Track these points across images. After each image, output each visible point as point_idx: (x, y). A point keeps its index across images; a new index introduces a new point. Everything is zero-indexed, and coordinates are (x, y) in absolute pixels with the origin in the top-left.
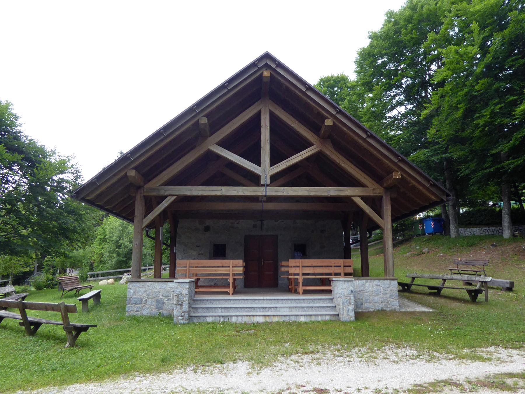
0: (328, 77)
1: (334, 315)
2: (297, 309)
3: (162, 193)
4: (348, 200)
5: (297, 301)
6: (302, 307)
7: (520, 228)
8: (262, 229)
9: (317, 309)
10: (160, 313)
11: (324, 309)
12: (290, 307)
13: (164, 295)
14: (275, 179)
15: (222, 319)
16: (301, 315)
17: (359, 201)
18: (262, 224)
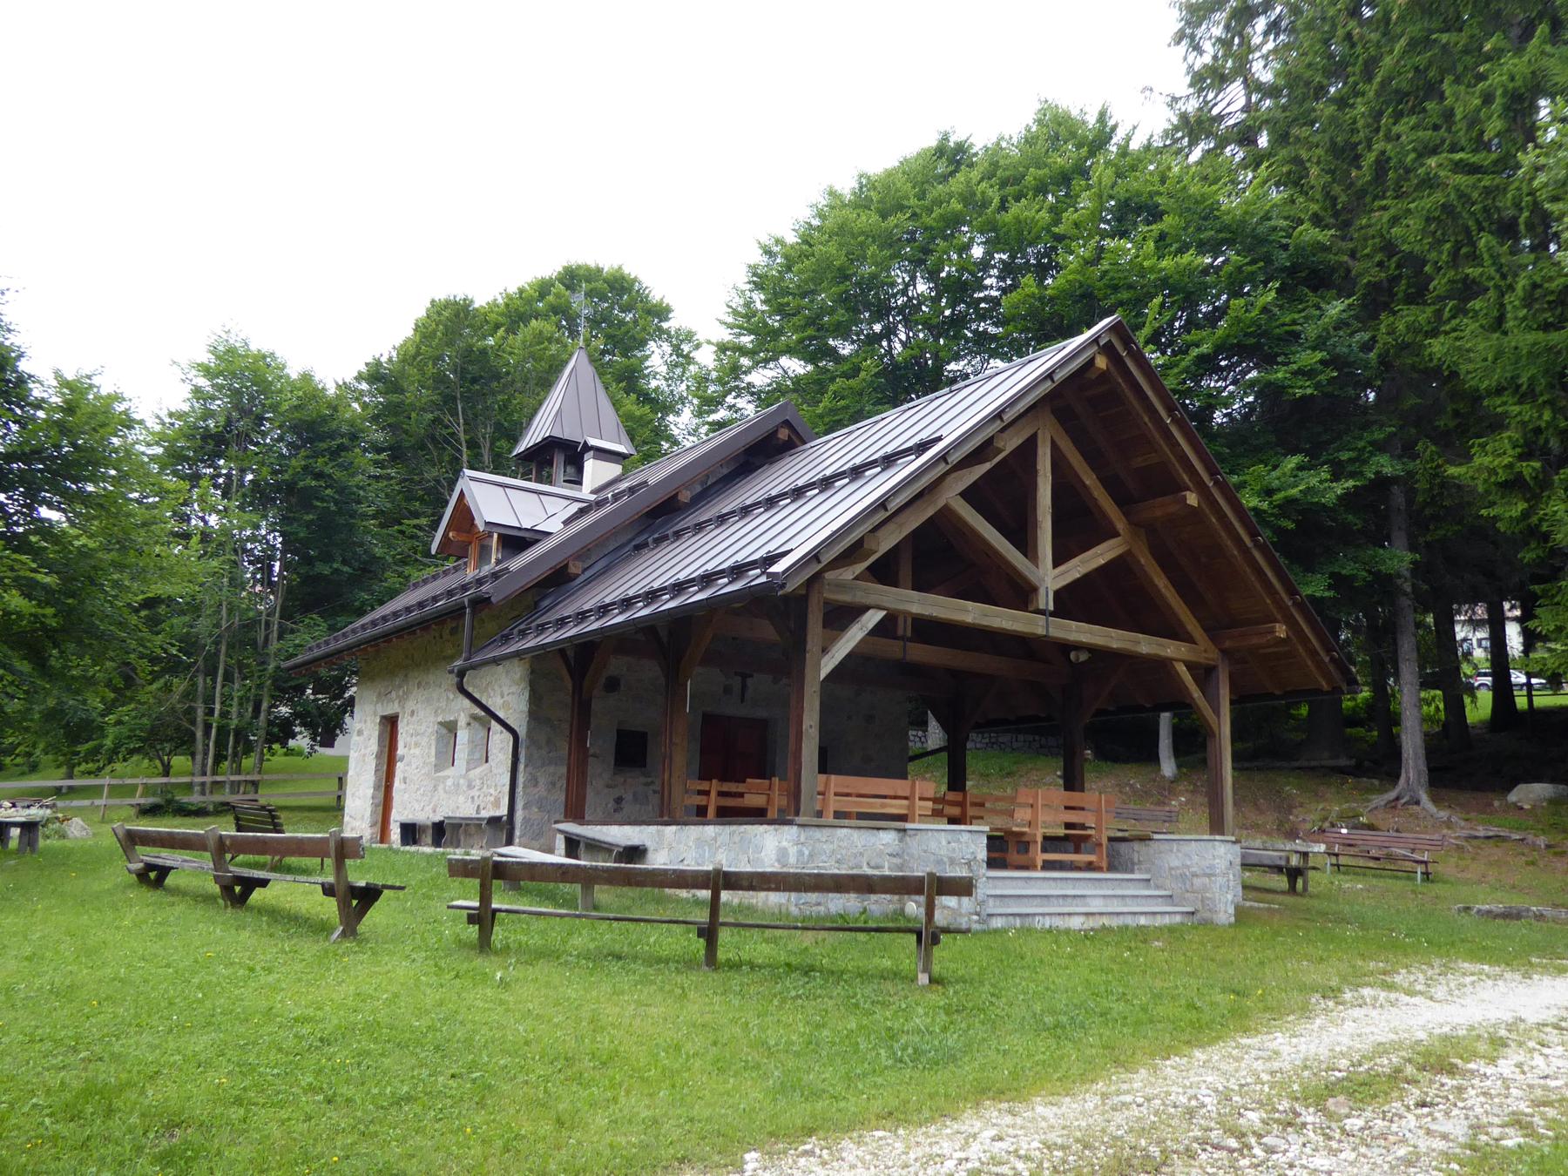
0: (588, 269)
1: (1187, 913)
2: (1115, 901)
3: (859, 598)
4: (1161, 666)
5: (1097, 883)
6: (1123, 897)
7: (1001, 740)
8: (742, 701)
9: (1144, 901)
10: (865, 910)
11: (1155, 901)
12: (1104, 896)
13: (872, 864)
14: (1071, 602)
15: (1018, 922)
16: (1142, 913)
17: (1182, 669)
18: (744, 687)
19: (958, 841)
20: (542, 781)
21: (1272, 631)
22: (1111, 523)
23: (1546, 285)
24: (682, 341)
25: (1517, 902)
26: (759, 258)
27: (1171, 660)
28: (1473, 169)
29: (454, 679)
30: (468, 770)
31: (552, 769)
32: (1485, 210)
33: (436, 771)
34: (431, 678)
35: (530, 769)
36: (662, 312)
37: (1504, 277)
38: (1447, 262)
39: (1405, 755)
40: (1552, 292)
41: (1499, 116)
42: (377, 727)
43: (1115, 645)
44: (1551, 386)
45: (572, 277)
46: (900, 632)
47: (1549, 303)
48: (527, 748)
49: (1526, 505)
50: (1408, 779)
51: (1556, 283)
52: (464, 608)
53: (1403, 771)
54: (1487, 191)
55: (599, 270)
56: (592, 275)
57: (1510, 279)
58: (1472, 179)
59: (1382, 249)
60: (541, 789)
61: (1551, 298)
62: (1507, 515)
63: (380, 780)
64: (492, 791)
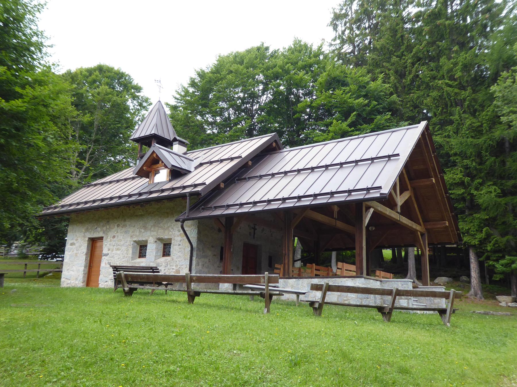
0: (108, 67)
8: (254, 238)
19: (407, 284)
20: (200, 264)
21: (445, 224)
22: (407, 187)
23: (473, 125)
24: (143, 101)
25: (487, 311)
26: (195, 76)
27: (417, 231)
28: (450, 86)
29: (179, 224)
30: (155, 259)
31: (203, 259)
32: (455, 99)
33: (132, 260)
34: (128, 223)
35: (197, 259)
36: (138, 89)
37: (461, 120)
38: (439, 113)
39: (409, 267)
40: (474, 127)
41: (460, 71)
42: (87, 242)
43: (410, 225)
44: (475, 156)
45: (100, 69)
46: (335, 217)
47: (473, 130)
48: (197, 251)
49: (464, 191)
50: (411, 275)
51: (476, 124)
52: (186, 196)
53: (409, 272)
54: (456, 94)
55: (113, 69)
56: (110, 70)
57: (463, 122)
58: (451, 89)
59: (412, 106)
60: (200, 267)
61: (474, 129)
62: (458, 193)
63: (87, 264)
64: (174, 267)
